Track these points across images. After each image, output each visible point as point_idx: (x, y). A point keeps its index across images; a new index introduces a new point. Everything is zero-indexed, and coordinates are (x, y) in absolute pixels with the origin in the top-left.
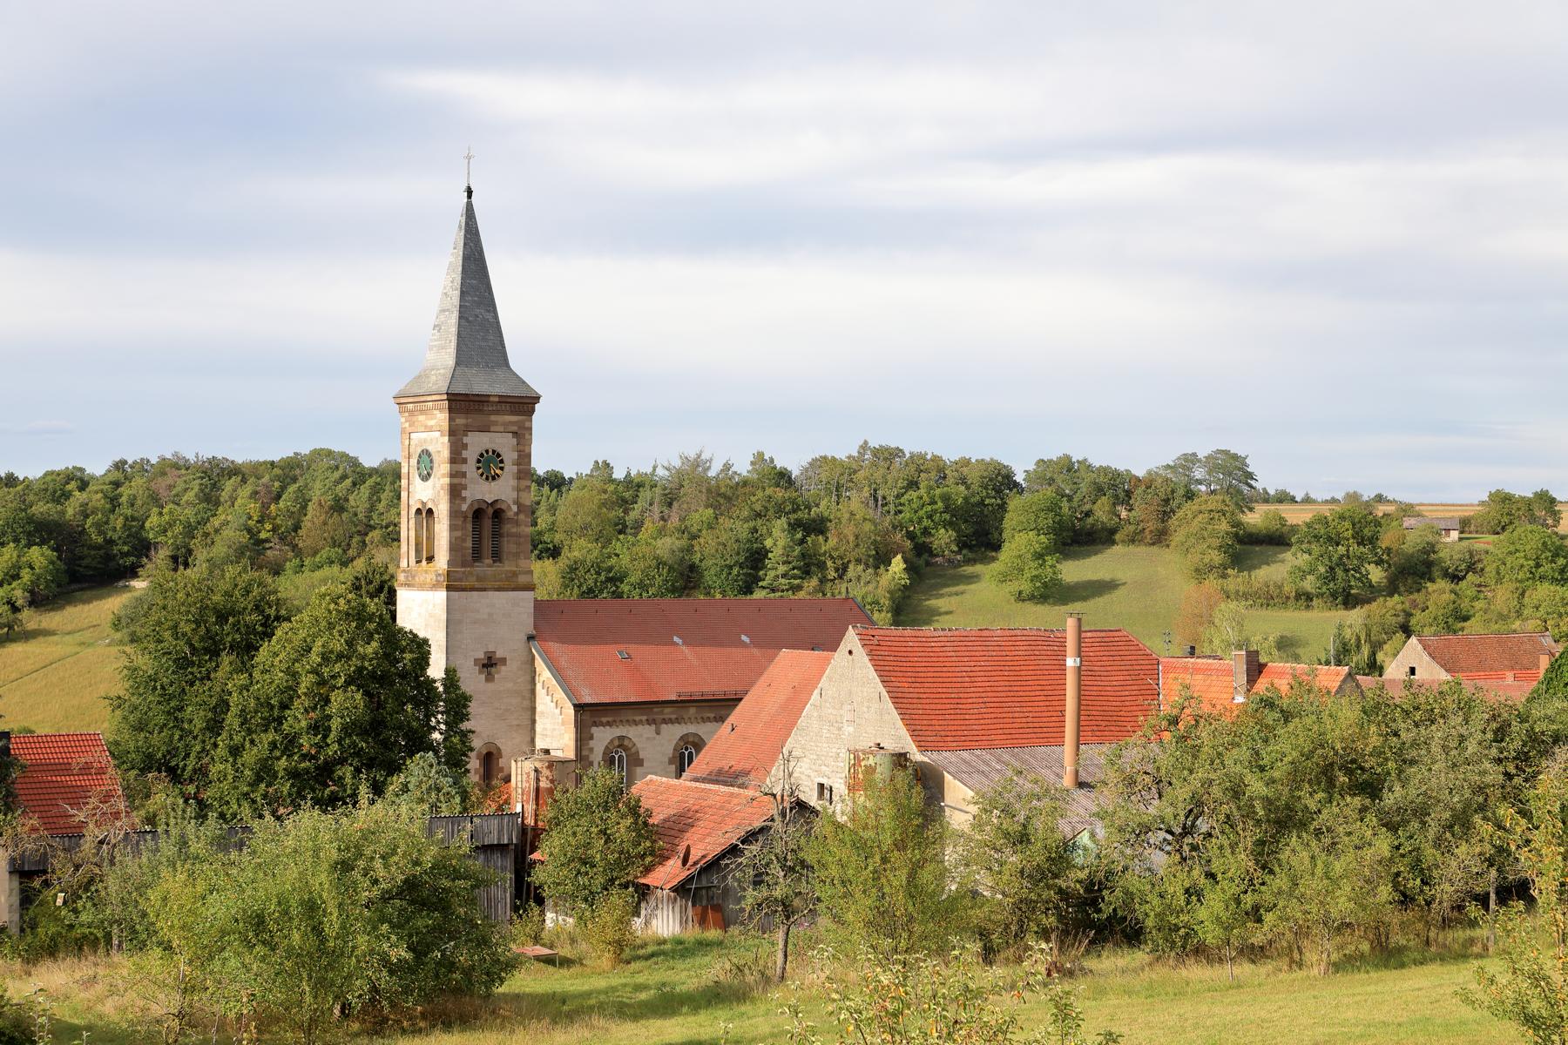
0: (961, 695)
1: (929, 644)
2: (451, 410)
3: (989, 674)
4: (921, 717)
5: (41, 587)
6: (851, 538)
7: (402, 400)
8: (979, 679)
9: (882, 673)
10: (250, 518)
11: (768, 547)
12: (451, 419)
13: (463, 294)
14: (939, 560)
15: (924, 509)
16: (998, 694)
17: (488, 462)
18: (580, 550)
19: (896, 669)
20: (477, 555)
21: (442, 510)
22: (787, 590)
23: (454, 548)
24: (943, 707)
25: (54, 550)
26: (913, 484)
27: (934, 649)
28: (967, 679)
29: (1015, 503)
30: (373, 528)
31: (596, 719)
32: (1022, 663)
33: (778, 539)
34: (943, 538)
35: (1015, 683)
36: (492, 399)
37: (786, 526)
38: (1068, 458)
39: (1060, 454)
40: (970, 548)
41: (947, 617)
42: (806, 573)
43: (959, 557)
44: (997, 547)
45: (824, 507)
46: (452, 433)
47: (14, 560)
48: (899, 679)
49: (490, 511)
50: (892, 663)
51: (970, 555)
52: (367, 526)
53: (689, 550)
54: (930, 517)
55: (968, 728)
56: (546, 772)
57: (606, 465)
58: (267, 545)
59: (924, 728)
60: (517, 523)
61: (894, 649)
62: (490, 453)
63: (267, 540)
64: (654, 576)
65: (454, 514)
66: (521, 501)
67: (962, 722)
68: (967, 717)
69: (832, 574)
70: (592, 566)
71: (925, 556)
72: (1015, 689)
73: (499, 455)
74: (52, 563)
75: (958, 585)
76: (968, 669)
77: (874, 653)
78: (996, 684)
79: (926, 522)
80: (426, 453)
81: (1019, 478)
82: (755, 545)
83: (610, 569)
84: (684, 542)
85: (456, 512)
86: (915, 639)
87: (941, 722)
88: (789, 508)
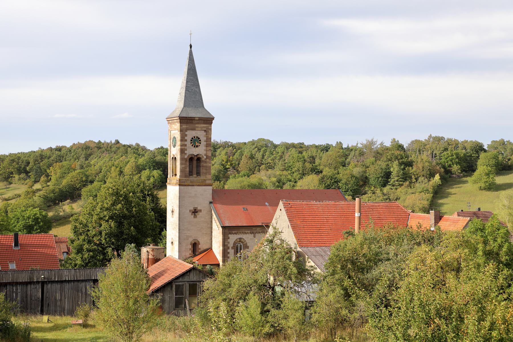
0: (322, 226)
1: (312, 207)
2: (181, 123)
3: (335, 218)
4: (303, 234)
5: (157, 183)
6: (421, 168)
7: (168, 119)
8: (331, 220)
9: (290, 218)
10: (223, 161)
11: (392, 171)
12: (181, 126)
13: (187, 82)
14: (454, 175)
15: (449, 158)
16: (337, 226)
17: (195, 141)
18: (327, 171)
19: (296, 216)
20: (191, 173)
21: (178, 158)
22: (398, 186)
23: (181, 171)
24: (313, 230)
25: (161, 171)
26: (446, 149)
27: (314, 209)
28: (326, 220)
29: (482, 155)
30: (263, 164)
31: (230, 232)
32: (350, 214)
33: (395, 168)
34: (455, 168)
35: (345, 222)
36: (196, 119)
37: (398, 164)
38: (503, 140)
39: (500, 139)
40: (466, 171)
41: (454, 195)
42: (405, 180)
43: (461, 175)
44: (474, 171)
45: (413, 158)
46: (181, 131)
47: (148, 174)
48: (297, 220)
49: (196, 158)
50: (295, 214)
51: (466, 174)
52: (261, 163)
53: (365, 172)
54: (451, 160)
55: (322, 238)
56: (151, 253)
57: (341, 143)
58: (229, 170)
59: (303, 238)
60: (206, 162)
61: (297, 209)
62: (196, 138)
63: (229, 168)
64: (350, 181)
65: (182, 159)
66: (208, 154)
67: (320, 236)
68: (322, 234)
69: (414, 180)
70: (329, 177)
71: (449, 174)
72: (345, 224)
73: (199, 138)
74: (161, 175)
75: (460, 184)
76: (327, 216)
77: (288, 210)
78: (337, 222)
79: (450, 163)
80: (174, 138)
81: (485, 147)
82: (388, 170)
83: (336, 178)
84: (364, 169)
85: (183, 158)
86: (307, 205)
87: (311, 236)
88: (399, 157)
